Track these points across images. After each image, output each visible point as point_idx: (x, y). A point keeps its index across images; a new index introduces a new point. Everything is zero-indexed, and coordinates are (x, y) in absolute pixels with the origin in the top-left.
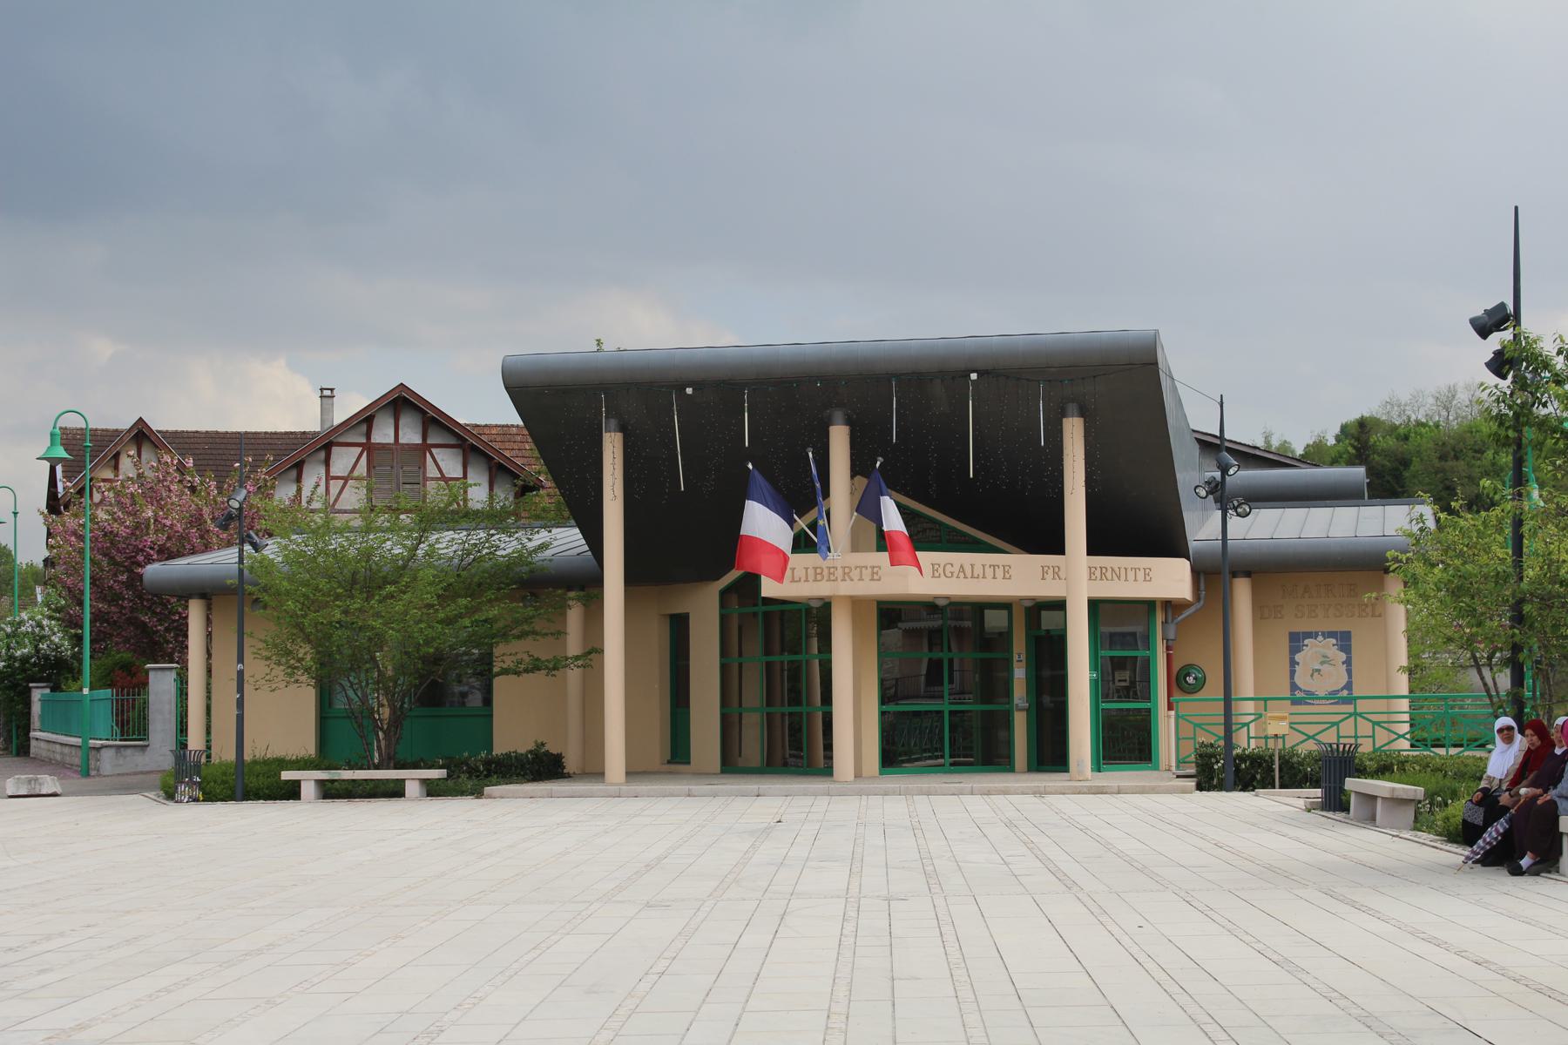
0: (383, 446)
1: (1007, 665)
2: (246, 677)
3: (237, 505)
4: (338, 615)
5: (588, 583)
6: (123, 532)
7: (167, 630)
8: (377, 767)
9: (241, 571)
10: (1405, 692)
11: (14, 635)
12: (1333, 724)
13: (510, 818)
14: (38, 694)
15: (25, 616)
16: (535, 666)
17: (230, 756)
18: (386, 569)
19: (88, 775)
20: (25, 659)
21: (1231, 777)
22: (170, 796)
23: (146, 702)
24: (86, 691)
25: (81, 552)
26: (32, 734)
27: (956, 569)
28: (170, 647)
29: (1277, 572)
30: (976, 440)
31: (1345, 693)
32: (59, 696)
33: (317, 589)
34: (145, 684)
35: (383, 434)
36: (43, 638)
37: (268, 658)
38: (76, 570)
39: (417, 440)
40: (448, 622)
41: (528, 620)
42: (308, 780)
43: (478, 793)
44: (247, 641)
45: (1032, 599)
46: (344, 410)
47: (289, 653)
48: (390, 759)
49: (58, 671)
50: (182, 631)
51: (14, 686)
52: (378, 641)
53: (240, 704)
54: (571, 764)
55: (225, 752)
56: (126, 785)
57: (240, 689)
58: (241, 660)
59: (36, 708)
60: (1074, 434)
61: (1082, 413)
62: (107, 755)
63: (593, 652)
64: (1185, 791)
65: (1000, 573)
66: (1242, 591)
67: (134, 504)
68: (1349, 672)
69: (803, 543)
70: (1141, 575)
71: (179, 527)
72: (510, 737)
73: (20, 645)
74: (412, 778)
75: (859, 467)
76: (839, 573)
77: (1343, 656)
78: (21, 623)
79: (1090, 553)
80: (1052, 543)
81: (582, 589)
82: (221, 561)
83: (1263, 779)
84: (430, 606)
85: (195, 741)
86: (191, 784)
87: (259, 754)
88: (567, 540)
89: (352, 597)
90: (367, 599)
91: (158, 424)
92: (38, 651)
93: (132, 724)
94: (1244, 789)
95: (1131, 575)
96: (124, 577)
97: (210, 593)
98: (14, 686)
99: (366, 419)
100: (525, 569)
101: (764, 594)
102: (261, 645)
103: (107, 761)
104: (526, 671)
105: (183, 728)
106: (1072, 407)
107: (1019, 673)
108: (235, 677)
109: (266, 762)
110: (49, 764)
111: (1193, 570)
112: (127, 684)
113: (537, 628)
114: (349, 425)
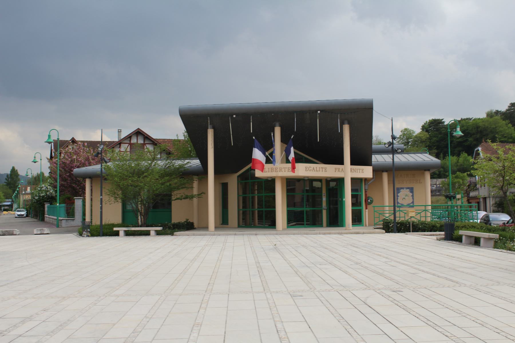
0: (133, 144)
1: (321, 197)
2: (103, 200)
3: (100, 150)
4: (130, 182)
5: (203, 173)
6: (68, 162)
7: (80, 188)
8: (141, 226)
9: (101, 169)
10: (430, 204)
11: (40, 190)
12: (419, 213)
13: (181, 241)
14: (47, 205)
15: (43, 185)
16: (186, 198)
17: (98, 223)
18: (143, 169)
19: (58, 227)
20: (43, 197)
21: (395, 229)
22: (81, 235)
23: (74, 208)
24: (58, 204)
25: (57, 167)
26: (45, 216)
27: (312, 168)
28: (81, 193)
29: (393, 170)
30: (326, 130)
31: (412, 204)
32: (52, 206)
33: (124, 175)
34: (74, 203)
35: (134, 140)
36: (48, 191)
37: (109, 195)
38: (55, 173)
39: (142, 142)
40: (163, 184)
41: (184, 184)
42: (122, 230)
43: (172, 234)
44: (103, 190)
45: (330, 178)
46: (124, 135)
47: (115, 193)
48: (145, 224)
49: (51, 200)
50: (84, 188)
51: (40, 203)
52: (142, 188)
53: (101, 208)
54: (196, 225)
55: (96, 222)
56: (68, 231)
57: (101, 204)
58: (101, 195)
59: (46, 209)
60: (346, 129)
61: (349, 124)
62: (64, 222)
63: (203, 194)
64: (382, 233)
65: (324, 170)
66: (385, 176)
67: (71, 155)
68: (413, 198)
69: (268, 161)
70: (361, 171)
71: (83, 161)
72: (177, 217)
73: (42, 193)
74: (152, 230)
75: (284, 140)
76: (278, 169)
77: (411, 194)
78: (42, 187)
79: (351, 164)
80: (340, 161)
81: (197, 176)
82: (96, 168)
83: (404, 229)
84: (157, 179)
85: (88, 219)
86: (87, 231)
87: (107, 223)
88: (195, 163)
89: (133, 177)
90: (139, 177)
91: (77, 139)
92: (47, 194)
93: (70, 213)
94: (398, 232)
95: (358, 171)
96: (68, 174)
97: (92, 177)
98: (40, 203)
99: (129, 137)
100: (183, 169)
101: (256, 176)
102: (108, 191)
103: (64, 224)
104: (184, 198)
105: (84, 214)
106: (346, 122)
107: (324, 199)
108: (100, 200)
109: (109, 225)
110: (50, 224)
111: (373, 171)
112: (69, 203)
113: (186, 186)
114: (125, 138)
